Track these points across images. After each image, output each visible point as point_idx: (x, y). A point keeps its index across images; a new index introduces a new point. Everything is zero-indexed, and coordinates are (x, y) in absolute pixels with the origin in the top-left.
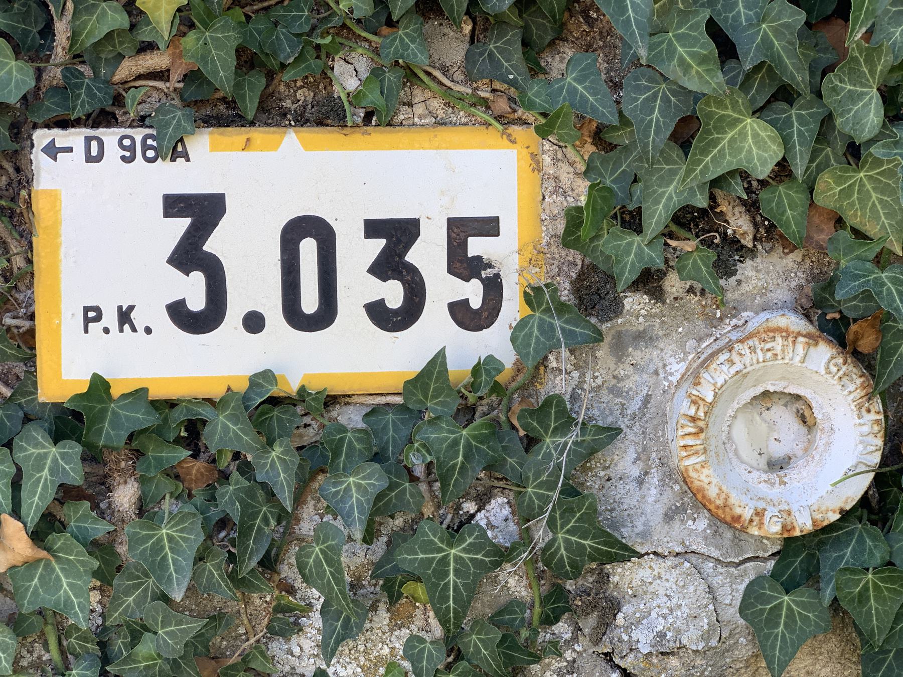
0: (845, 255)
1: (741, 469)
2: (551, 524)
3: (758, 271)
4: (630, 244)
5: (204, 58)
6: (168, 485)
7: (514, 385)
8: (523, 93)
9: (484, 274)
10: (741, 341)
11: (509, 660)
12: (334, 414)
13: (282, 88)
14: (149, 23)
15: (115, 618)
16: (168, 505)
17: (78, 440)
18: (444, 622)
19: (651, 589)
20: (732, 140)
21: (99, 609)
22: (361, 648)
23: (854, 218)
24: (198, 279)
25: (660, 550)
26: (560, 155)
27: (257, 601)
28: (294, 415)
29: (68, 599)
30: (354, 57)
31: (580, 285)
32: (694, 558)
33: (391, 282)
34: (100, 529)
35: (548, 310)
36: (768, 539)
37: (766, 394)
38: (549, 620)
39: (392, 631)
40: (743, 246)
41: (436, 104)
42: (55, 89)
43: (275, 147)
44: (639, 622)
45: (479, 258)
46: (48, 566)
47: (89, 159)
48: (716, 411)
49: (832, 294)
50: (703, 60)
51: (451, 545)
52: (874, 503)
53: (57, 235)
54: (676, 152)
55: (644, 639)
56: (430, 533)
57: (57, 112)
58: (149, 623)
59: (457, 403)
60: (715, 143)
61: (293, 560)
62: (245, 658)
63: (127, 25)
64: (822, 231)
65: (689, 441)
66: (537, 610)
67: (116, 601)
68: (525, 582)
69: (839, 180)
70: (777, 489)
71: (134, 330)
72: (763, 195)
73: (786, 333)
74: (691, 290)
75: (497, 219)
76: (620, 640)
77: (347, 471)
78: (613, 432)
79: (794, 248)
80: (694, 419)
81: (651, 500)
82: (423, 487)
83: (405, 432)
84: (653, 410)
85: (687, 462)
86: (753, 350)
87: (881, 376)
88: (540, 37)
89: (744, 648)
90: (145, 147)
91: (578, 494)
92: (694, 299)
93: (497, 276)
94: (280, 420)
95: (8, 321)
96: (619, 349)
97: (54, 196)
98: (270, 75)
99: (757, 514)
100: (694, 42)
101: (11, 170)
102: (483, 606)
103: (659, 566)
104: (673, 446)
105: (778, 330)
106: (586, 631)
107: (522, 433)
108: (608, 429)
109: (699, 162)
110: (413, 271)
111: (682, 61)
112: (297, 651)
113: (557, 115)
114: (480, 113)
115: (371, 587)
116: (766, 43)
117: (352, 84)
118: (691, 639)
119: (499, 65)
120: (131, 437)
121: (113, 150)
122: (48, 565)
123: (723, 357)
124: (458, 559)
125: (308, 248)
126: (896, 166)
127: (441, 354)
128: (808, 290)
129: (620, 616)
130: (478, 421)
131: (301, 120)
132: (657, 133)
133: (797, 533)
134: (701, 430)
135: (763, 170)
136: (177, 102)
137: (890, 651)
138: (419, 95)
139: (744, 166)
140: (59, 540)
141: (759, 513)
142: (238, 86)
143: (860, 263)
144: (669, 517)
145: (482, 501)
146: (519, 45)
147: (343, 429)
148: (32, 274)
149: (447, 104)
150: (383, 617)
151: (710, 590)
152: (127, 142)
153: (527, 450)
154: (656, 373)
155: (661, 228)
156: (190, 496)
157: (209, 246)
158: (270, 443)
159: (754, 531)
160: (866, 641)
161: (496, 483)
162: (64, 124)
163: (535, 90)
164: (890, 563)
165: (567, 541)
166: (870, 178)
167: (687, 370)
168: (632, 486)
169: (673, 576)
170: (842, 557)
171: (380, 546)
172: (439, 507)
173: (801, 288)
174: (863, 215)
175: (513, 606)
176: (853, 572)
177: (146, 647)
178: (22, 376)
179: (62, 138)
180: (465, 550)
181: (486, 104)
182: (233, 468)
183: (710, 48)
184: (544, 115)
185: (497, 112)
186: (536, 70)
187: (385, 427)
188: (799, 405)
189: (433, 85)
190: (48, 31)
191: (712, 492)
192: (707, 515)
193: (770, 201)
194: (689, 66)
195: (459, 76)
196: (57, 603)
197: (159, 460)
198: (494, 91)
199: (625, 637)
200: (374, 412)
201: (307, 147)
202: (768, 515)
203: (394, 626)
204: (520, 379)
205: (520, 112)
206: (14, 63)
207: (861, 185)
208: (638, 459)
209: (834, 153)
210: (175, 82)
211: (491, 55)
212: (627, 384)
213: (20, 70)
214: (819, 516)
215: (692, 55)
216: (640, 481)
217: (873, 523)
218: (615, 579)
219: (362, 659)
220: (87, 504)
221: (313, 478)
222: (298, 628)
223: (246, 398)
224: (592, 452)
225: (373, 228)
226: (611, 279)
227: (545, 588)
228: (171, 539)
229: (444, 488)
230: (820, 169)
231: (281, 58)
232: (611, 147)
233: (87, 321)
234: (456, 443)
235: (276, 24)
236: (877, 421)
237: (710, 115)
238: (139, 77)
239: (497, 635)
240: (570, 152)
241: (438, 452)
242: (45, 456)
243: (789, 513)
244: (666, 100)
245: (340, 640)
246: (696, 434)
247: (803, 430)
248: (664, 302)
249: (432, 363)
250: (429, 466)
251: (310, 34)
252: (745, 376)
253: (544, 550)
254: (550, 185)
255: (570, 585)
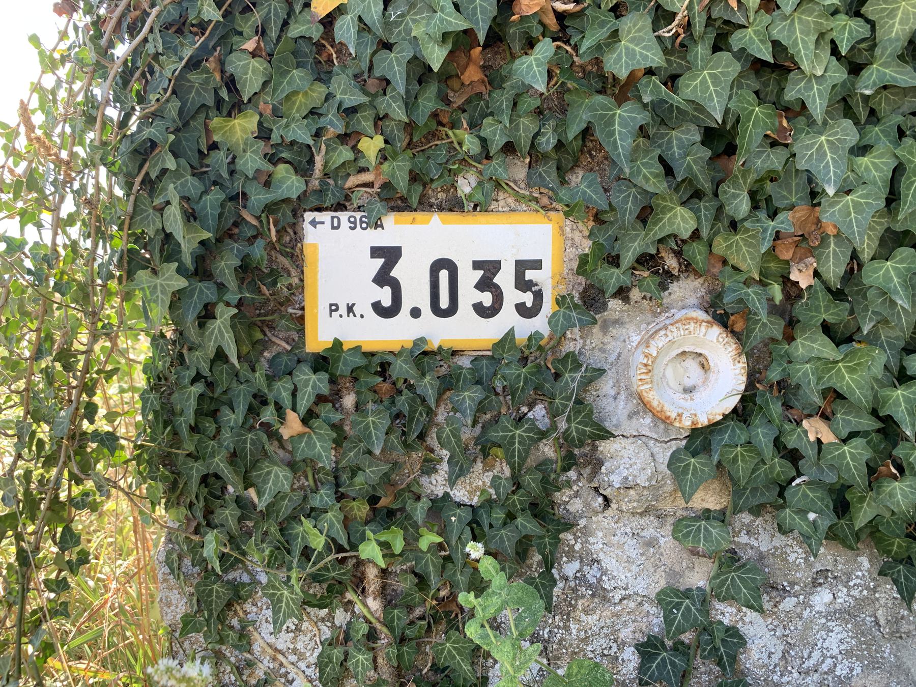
0: (728, 279)
1: (670, 392)
2: (568, 420)
3: (680, 288)
4: (613, 273)
5: (393, 176)
6: (370, 396)
7: (548, 346)
8: (556, 193)
9: (533, 289)
10: (672, 325)
11: (545, 489)
12: (455, 360)
13: (430, 192)
14: (364, 157)
15: (343, 463)
16: (370, 406)
17: (326, 372)
18: (512, 468)
19: (620, 454)
20: (670, 219)
21: (334, 459)
22: (468, 481)
23: (733, 260)
24: (387, 290)
25: (625, 434)
26: (575, 227)
27: (415, 456)
28: (436, 360)
29: (320, 454)
30: (468, 176)
31: (584, 295)
32: (643, 438)
33: (485, 293)
34: (336, 417)
35: (568, 308)
36: (683, 428)
37: (684, 353)
38: (566, 469)
39: (484, 473)
40: (673, 275)
41: (511, 201)
42: (315, 191)
43: (427, 222)
44: (614, 471)
45: (531, 281)
46: (310, 437)
47: (333, 228)
48: (657, 361)
49: (721, 300)
50: (656, 176)
51: (516, 429)
52: (740, 411)
53: (316, 267)
54: (639, 225)
55: (616, 480)
56: (506, 422)
57: (315, 203)
58: (362, 466)
59: (519, 355)
60: (661, 219)
61: (434, 436)
62: (408, 486)
63: (353, 158)
64: (715, 267)
65: (643, 377)
66: (559, 464)
67: (344, 455)
68: (553, 449)
69: (726, 240)
70: (689, 403)
71: (355, 316)
72: (685, 248)
73: (696, 320)
74: (644, 298)
75: (541, 261)
76: (603, 481)
77: (463, 389)
78: (601, 372)
79: (701, 276)
80: (646, 365)
81: (621, 407)
82: (501, 398)
83: (492, 370)
84: (622, 361)
85: (642, 388)
86: (678, 329)
87: (746, 344)
88: (566, 165)
89: (669, 486)
90: (362, 222)
91: (582, 403)
92: (646, 302)
93: (540, 290)
94: (428, 363)
95: (290, 310)
96: (605, 329)
97: (315, 246)
98: (425, 185)
99: (679, 415)
100: (652, 166)
101: (292, 233)
102: (531, 462)
103: (624, 442)
104: (634, 380)
105: (692, 319)
106: (585, 475)
107: (553, 371)
108: (599, 370)
109: (652, 230)
110: (497, 287)
111: (645, 177)
112: (434, 482)
113: (575, 206)
114: (533, 205)
115: (474, 450)
116: (689, 167)
117: (467, 190)
118: (642, 480)
119: (544, 179)
120: (352, 372)
121: (345, 224)
122: (310, 436)
123: (662, 333)
124: (520, 436)
125: (444, 275)
126: (757, 233)
127: (512, 330)
128: (708, 298)
129: (603, 468)
130: (529, 365)
131: (441, 209)
132: (630, 214)
133: (700, 426)
134: (650, 371)
135: (686, 235)
136: (377, 199)
137: (445, 551)
138: (501, 195)
139: (676, 232)
140: (316, 423)
141: (680, 415)
142: (409, 191)
143: (736, 284)
144: (630, 417)
145: (531, 406)
146: (555, 169)
147: (461, 368)
148: (303, 287)
149: (516, 200)
150: (479, 466)
151: (652, 455)
152: (352, 219)
153: (555, 380)
154: (624, 341)
155: (630, 265)
156: (382, 401)
157: (394, 273)
158: (424, 375)
159: (677, 424)
160: (734, 481)
161: (538, 397)
162: (319, 209)
163: (563, 193)
164: (749, 442)
165: (576, 428)
166: (742, 239)
167: (642, 339)
168: (611, 400)
169: (632, 448)
170: (723, 439)
171: (478, 429)
172: (509, 409)
173: (703, 297)
174: (738, 259)
175: (547, 461)
176: (730, 446)
177: (359, 479)
178: (296, 339)
179: (319, 216)
180: (524, 431)
181: (537, 200)
182: (403, 387)
183: (660, 169)
184: (567, 206)
185: (543, 205)
186: (563, 182)
187: (482, 367)
188: (701, 359)
189: (509, 190)
190: (311, 161)
191: (655, 404)
192: (651, 414)
193: (688, 251)
194: (649, 179)
195: (522, 185)
196: (314, 455)
197: (366, 383)
198: (541, 193)
199: (606, 479)
200: (477, 359)
201: (444, 222)
202: (684, 416)
203: (485, 471)
204: (551, 343)
205: (554, 204)
206: (294, 177)
207: (738, 243)
208: (614, 386)
209: (724, 227)
210: (376, 189)
211: (540, 174)
212: (608, 347)
213: (298, 181)
214: (711, 417)
215: (651, 173)
216: (615, 398)
217: (740, 421)
218: (600, 449)
219: (468, 487)
220: (331, 405)
221: (444, 393)
222: (435, 471)
223: (411, 351)
224: (590, 381)
225: (477, 265)
226: (603, 292)
227: (564, 453)
228: (374, 423)
229: (513, 399)
230: (715, 234)
231: (431, 176)
232: (604, 222)
233: (331, 311)
234: (519, 375)
235: (429, 158)
236: (744, 368)
237: (658, 205)
238: (358, 186)
239: (540, 476)
240: (580, 225)
241: (510, 380)
242: (310, 379)
243: (696, 416)
244: (635, 197)
245: (458, 477)
246: (647, 373)
247: (702, 372)
248: (629, 304)
249: (507, 334)
250: (504, 388)
251: (447, 163)
252: (674, 343)
253: (564, 433)
254: (569, 243)
255: (576, 451)
